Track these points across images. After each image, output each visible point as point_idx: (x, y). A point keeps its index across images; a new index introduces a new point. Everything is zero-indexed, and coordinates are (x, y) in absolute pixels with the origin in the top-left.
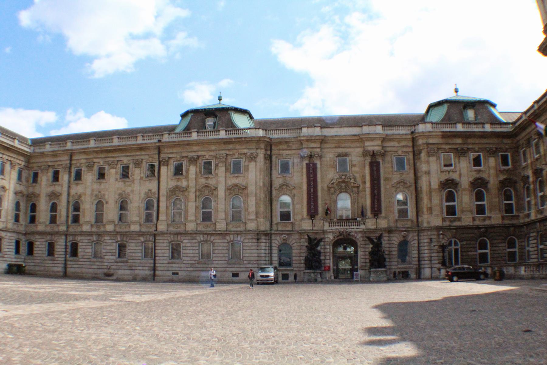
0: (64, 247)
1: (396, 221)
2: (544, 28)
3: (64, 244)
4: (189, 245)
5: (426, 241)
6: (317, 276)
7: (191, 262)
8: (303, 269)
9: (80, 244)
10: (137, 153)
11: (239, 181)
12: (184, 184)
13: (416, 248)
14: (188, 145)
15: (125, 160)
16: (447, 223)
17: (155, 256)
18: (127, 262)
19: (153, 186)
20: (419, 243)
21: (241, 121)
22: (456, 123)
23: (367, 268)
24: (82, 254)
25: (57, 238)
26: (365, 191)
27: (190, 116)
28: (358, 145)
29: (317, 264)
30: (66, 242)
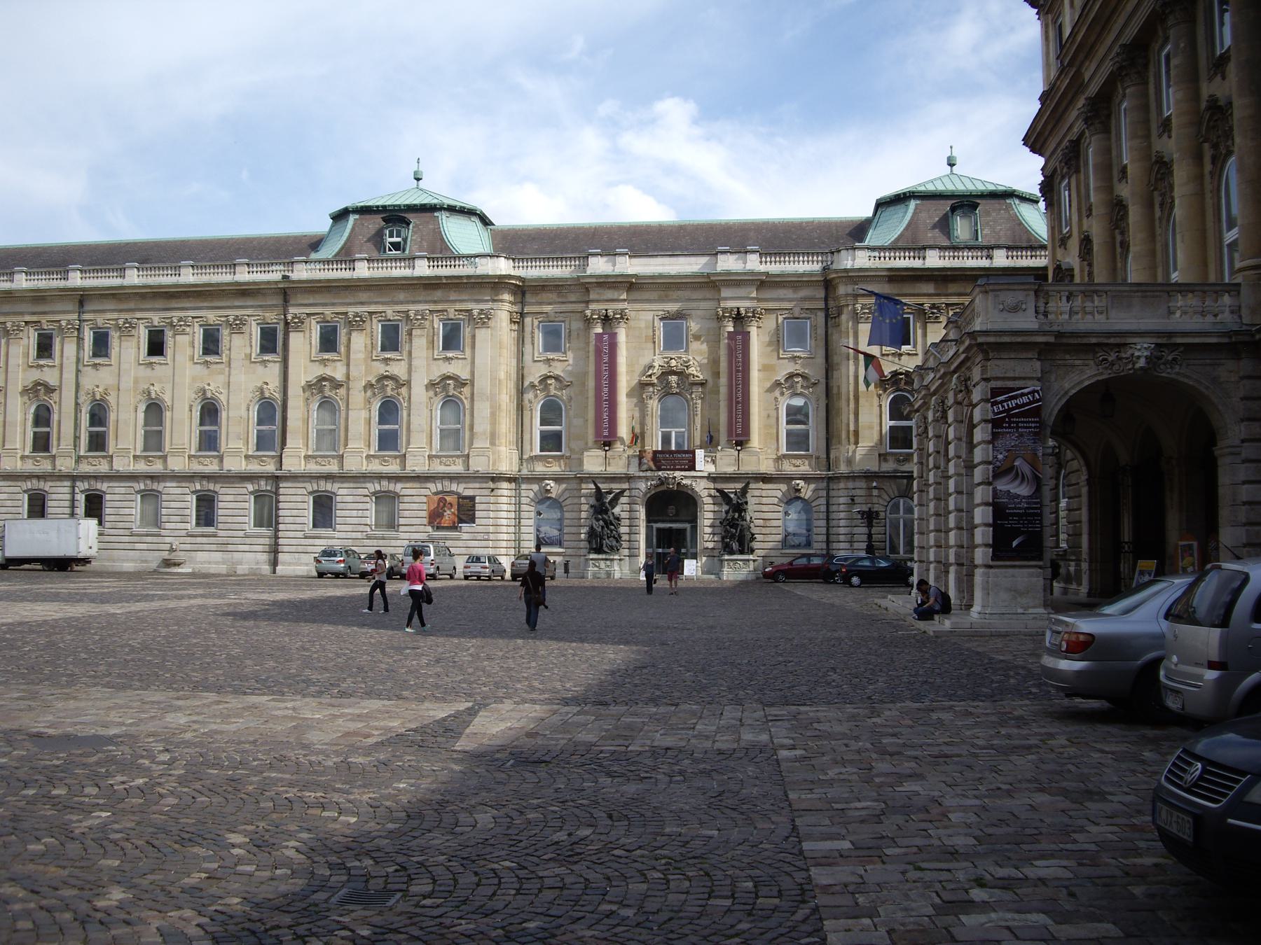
0: (67, 504)
1: (780, 459)
2: (1044, 98)
3: (68, 497)
4: (349, 499)
5: (842, 500)
6: (612, 566)
7: (354, 535)
8: (583, 552)
9: (108, 497)
10: (237, 303)
11: (459, 369)
12: (338, 373)
13: (823, 516)
14: (346, 288)
15: (212, 316)
16: (889, 466)
17: (278, 523)
18: (738, 371)
19: (271, 375)
20: (828, 504)
21: (462, 236)
22: (924, 248)
23: (716, 553)
24: (112, 518)
25: (50, 484)
26: (718, 392)
27: (352, 218)
28: (708, 296)
29: (614, 543)
30: (73, 493)
